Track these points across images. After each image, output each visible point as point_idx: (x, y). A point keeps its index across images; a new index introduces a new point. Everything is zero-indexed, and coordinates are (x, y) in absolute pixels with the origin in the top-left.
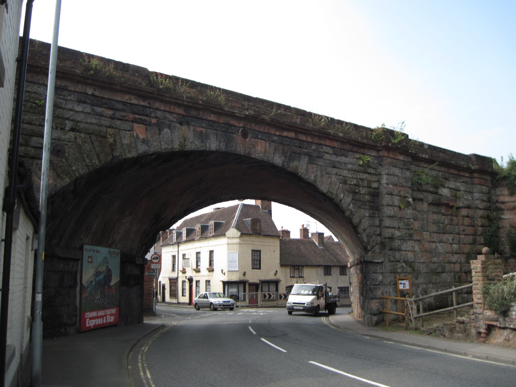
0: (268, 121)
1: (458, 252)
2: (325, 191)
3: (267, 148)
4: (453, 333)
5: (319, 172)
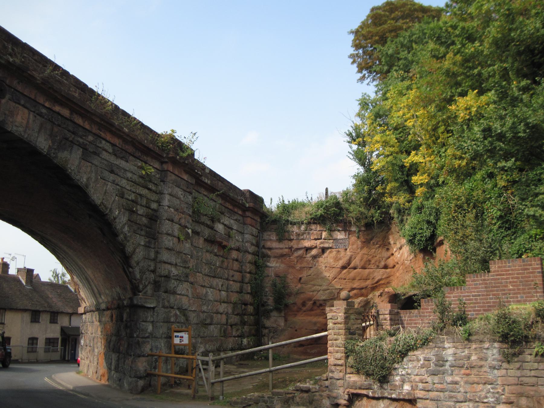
0: (38, 82)
1: (226, 300)
2: (98, 202)
3: (31, 121)
4: (289, 405)
5: (93, 174)
